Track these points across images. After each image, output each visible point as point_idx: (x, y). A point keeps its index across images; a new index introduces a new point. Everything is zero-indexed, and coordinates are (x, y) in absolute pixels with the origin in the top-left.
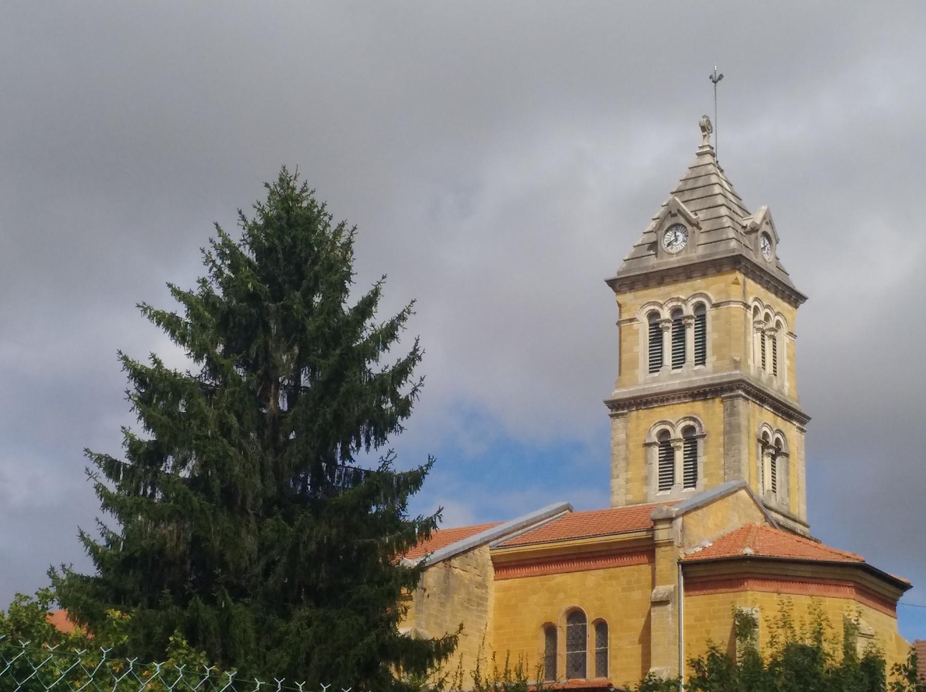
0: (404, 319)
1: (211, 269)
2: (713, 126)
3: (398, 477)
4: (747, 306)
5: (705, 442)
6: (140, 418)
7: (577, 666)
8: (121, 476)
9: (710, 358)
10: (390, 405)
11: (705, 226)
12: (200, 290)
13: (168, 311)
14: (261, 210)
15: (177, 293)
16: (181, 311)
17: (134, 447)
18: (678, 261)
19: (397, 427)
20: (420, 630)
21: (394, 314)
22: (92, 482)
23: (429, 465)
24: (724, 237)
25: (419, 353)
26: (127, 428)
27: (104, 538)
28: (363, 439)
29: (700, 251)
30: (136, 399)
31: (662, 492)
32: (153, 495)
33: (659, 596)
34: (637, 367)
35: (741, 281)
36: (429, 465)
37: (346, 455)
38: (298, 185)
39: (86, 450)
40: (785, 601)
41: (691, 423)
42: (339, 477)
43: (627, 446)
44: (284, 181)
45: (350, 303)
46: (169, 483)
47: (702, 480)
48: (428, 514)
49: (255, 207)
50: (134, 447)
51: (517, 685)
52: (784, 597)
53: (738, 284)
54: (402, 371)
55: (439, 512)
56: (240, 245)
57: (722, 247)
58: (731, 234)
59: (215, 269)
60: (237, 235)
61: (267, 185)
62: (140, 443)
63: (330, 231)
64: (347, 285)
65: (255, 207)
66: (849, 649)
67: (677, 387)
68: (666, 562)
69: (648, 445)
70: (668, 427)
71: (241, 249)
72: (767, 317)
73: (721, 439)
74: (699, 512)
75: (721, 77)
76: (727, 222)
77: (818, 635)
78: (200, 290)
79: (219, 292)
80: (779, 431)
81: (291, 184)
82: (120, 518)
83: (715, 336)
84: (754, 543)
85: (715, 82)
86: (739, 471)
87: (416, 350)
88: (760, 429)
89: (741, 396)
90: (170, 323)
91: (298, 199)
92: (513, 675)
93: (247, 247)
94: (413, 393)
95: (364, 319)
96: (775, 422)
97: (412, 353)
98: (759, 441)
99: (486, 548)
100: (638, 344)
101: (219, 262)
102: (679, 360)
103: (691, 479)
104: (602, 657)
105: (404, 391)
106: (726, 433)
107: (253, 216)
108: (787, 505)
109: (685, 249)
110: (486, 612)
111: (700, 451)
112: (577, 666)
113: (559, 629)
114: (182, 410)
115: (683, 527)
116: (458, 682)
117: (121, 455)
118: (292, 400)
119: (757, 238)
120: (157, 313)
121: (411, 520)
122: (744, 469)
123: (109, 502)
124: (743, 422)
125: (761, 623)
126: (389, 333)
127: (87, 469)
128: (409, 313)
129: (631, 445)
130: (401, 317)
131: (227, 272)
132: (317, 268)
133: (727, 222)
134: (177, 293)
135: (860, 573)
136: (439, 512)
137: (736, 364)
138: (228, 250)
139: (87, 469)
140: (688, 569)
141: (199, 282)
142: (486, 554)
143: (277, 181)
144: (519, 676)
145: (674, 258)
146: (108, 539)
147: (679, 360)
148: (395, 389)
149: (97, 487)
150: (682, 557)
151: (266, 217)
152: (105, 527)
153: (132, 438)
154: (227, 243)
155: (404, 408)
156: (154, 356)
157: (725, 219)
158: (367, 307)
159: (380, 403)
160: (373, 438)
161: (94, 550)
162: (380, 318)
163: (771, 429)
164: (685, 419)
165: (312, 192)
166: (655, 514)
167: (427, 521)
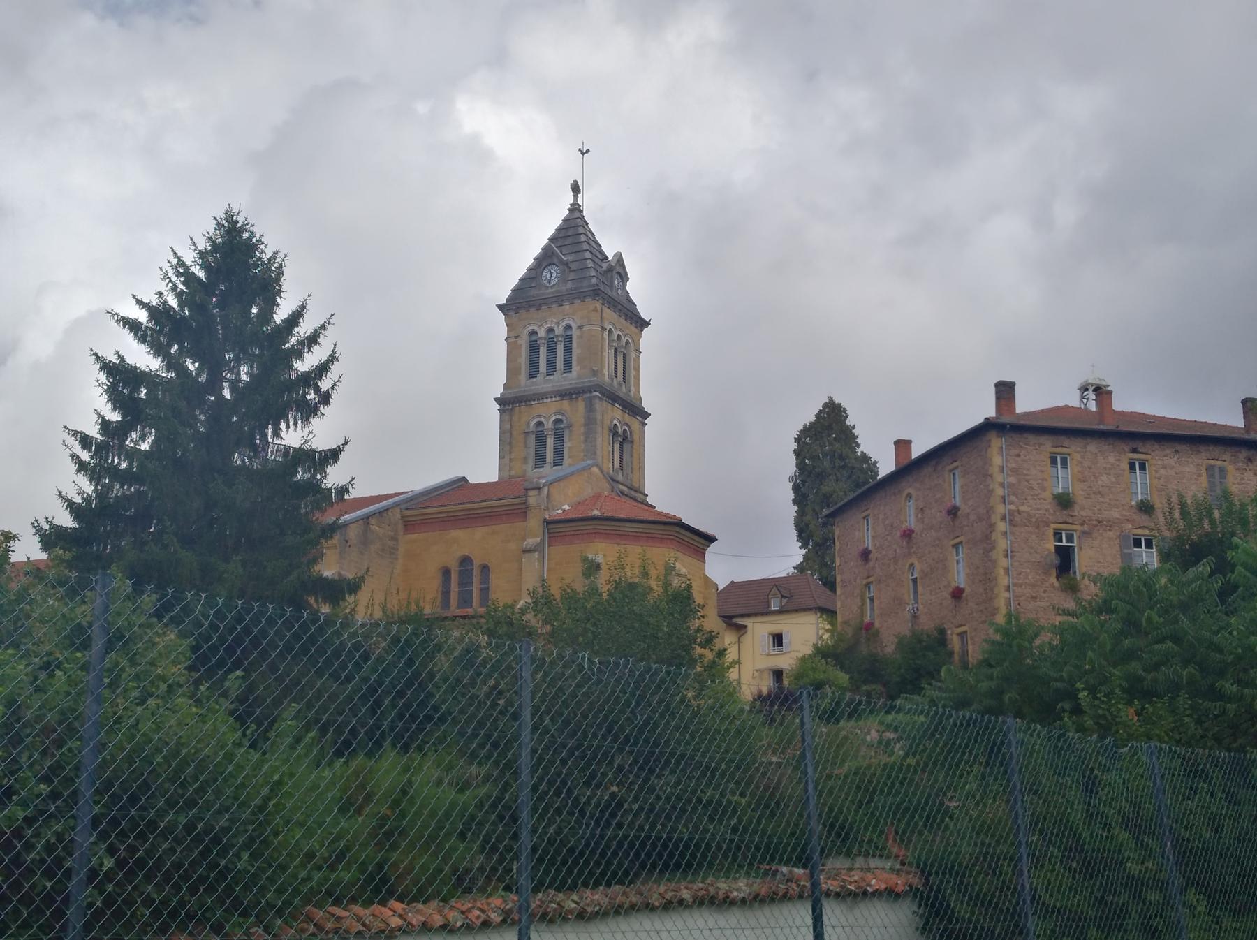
0: (325, 329)
1: (167, 284)
2: (581, 188)
3: (320, 453)
4: (604, 329)
5: (571, 431)
6: (108, 402)
7: (465, 601)
8: (93, 448)
9: (575, 368)
10: (313, 396)
11: (573, 267)
12: (157, 301)
13: (132, 317)
14: (210, 239)
15: (140, 303)
16: (142, 316)
17: (105, 425)
18: (552, 293)
19: (319, 413)
20: (343, 573)
21: (317, 325)
22: (68, 452)
23: (346, 444)
24: (587, 275)
25: (337, 355)
26: (99, 411)
27: (80, 497)
28: (291, 423)
29: (569, 285)
30: (105, 387)
31: (537, 470)
32: (119, 463)
33: (529, 547)
34: (520, 374)
35: (599, 309)
36: (346, 444)
37: (277, 434)
38: (241, 220)
39: (65, 427)
40: (623, 551)
41: (560, 417)
42: (272, 452)
43: (511, 434)
44: (229, 217)
45: (280, 315)
46: (132, 454)
47: (567, 460)
48: (342, 482)
49: (204, 235)
50: (105, 425)
51: (416, 614)
52: (622, 547)
53: (597, 311)
54: (323, 369)
55: (352, 480)
56: (191, 266)
57: (585, 283)
58: (593, 273)
59: (170, 284)
60: (190, 257)
61: (215, 219)
62: (109, 422)
63: (265, 258)
64: (278, 300)
65: (204, 235)
66: (666, 585)
67: (550, 389)
68: (534, 522)
69: (527, 433)
70: (543, 420)
71: (192, 269)
72: (619, 337)
73: (582, 430)
74: (562, 484)
75: (588, 151)
76: (590, 264)
77: (645, 574)
78: (157, 301)
79: (173, 302)
80: (626, 424)
81: (234, 218)
82: (91, 481)
83: (579, 351)
84: (601, 507)
85: (583, 154)
86: (595, 453)
87: (334, 353)
88: (611, 422)
89: (597, 396)
90: (133, 326)
91: (241, 230)
92: (413, 607)
93: (198, 267)
94: (333, 388)
95: (293, 328)
96: (623, 417)
97: (330, 356)
98: (610, 431)
99: (398, 510)
100: (521, 356)
101: (174, 278)
102: (551, 370)
103: (558, 460)
104: (485, 591)
105: (324, 385)
106: (586, 425)
107: (203, 244)
108: (631, 480)
109: (558, 283)
110: (397, 559)
111: (566, 438)
112: (465, 601)
113: (452, 572)
114: (143, 396)
115: (548, 494)
116: (369, 612)
117: (94, 431)
118: (233, 389)
119: (612, 277)
120: (123, 318)
121: (329, 486)
122: (599, 452)
123: (82, 466)
124: (599, 417)
125: (604, 567)
126: (313, 340)
127: (64, 441)
128: (329, 323)
129: (515, 433)
130: (323, 327)
131: (181, 287)
132: (254, 286)
133: (590, 264)
134: (140, 303)
135: (678, 529)
136: (352, 480)
137: (595, 373)
138: (182, 268)
139: (64, 441)
140: (550, 526)
141: (156, 294)
142: (397, 514)
143: (223, 216)
144: (417, 606)
145: (550, 290)
146: (83, 498)
147: (551, 370)
148: (317, 383)
149: (72, 456)
150: (547, 517)
151: (214, 244)
152: (81, 488)
153: (103, 418)
154: (181, 264)
155: (325, 398)
156: (118, 353)
157: (588, 261)
158: (295, 319)
159: (304, 394)
160: (300, 422)
161: (71, 505)
162: (304, 329)
163: (620, 423)
164: (555, 414)
165: (253, 226)
166: (527, 485)
167: (342, 487)
